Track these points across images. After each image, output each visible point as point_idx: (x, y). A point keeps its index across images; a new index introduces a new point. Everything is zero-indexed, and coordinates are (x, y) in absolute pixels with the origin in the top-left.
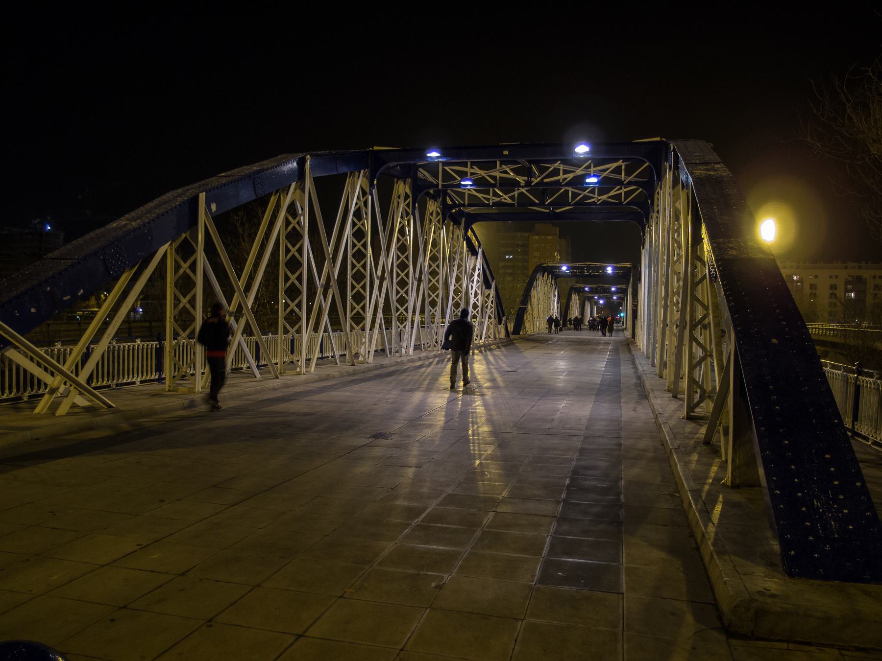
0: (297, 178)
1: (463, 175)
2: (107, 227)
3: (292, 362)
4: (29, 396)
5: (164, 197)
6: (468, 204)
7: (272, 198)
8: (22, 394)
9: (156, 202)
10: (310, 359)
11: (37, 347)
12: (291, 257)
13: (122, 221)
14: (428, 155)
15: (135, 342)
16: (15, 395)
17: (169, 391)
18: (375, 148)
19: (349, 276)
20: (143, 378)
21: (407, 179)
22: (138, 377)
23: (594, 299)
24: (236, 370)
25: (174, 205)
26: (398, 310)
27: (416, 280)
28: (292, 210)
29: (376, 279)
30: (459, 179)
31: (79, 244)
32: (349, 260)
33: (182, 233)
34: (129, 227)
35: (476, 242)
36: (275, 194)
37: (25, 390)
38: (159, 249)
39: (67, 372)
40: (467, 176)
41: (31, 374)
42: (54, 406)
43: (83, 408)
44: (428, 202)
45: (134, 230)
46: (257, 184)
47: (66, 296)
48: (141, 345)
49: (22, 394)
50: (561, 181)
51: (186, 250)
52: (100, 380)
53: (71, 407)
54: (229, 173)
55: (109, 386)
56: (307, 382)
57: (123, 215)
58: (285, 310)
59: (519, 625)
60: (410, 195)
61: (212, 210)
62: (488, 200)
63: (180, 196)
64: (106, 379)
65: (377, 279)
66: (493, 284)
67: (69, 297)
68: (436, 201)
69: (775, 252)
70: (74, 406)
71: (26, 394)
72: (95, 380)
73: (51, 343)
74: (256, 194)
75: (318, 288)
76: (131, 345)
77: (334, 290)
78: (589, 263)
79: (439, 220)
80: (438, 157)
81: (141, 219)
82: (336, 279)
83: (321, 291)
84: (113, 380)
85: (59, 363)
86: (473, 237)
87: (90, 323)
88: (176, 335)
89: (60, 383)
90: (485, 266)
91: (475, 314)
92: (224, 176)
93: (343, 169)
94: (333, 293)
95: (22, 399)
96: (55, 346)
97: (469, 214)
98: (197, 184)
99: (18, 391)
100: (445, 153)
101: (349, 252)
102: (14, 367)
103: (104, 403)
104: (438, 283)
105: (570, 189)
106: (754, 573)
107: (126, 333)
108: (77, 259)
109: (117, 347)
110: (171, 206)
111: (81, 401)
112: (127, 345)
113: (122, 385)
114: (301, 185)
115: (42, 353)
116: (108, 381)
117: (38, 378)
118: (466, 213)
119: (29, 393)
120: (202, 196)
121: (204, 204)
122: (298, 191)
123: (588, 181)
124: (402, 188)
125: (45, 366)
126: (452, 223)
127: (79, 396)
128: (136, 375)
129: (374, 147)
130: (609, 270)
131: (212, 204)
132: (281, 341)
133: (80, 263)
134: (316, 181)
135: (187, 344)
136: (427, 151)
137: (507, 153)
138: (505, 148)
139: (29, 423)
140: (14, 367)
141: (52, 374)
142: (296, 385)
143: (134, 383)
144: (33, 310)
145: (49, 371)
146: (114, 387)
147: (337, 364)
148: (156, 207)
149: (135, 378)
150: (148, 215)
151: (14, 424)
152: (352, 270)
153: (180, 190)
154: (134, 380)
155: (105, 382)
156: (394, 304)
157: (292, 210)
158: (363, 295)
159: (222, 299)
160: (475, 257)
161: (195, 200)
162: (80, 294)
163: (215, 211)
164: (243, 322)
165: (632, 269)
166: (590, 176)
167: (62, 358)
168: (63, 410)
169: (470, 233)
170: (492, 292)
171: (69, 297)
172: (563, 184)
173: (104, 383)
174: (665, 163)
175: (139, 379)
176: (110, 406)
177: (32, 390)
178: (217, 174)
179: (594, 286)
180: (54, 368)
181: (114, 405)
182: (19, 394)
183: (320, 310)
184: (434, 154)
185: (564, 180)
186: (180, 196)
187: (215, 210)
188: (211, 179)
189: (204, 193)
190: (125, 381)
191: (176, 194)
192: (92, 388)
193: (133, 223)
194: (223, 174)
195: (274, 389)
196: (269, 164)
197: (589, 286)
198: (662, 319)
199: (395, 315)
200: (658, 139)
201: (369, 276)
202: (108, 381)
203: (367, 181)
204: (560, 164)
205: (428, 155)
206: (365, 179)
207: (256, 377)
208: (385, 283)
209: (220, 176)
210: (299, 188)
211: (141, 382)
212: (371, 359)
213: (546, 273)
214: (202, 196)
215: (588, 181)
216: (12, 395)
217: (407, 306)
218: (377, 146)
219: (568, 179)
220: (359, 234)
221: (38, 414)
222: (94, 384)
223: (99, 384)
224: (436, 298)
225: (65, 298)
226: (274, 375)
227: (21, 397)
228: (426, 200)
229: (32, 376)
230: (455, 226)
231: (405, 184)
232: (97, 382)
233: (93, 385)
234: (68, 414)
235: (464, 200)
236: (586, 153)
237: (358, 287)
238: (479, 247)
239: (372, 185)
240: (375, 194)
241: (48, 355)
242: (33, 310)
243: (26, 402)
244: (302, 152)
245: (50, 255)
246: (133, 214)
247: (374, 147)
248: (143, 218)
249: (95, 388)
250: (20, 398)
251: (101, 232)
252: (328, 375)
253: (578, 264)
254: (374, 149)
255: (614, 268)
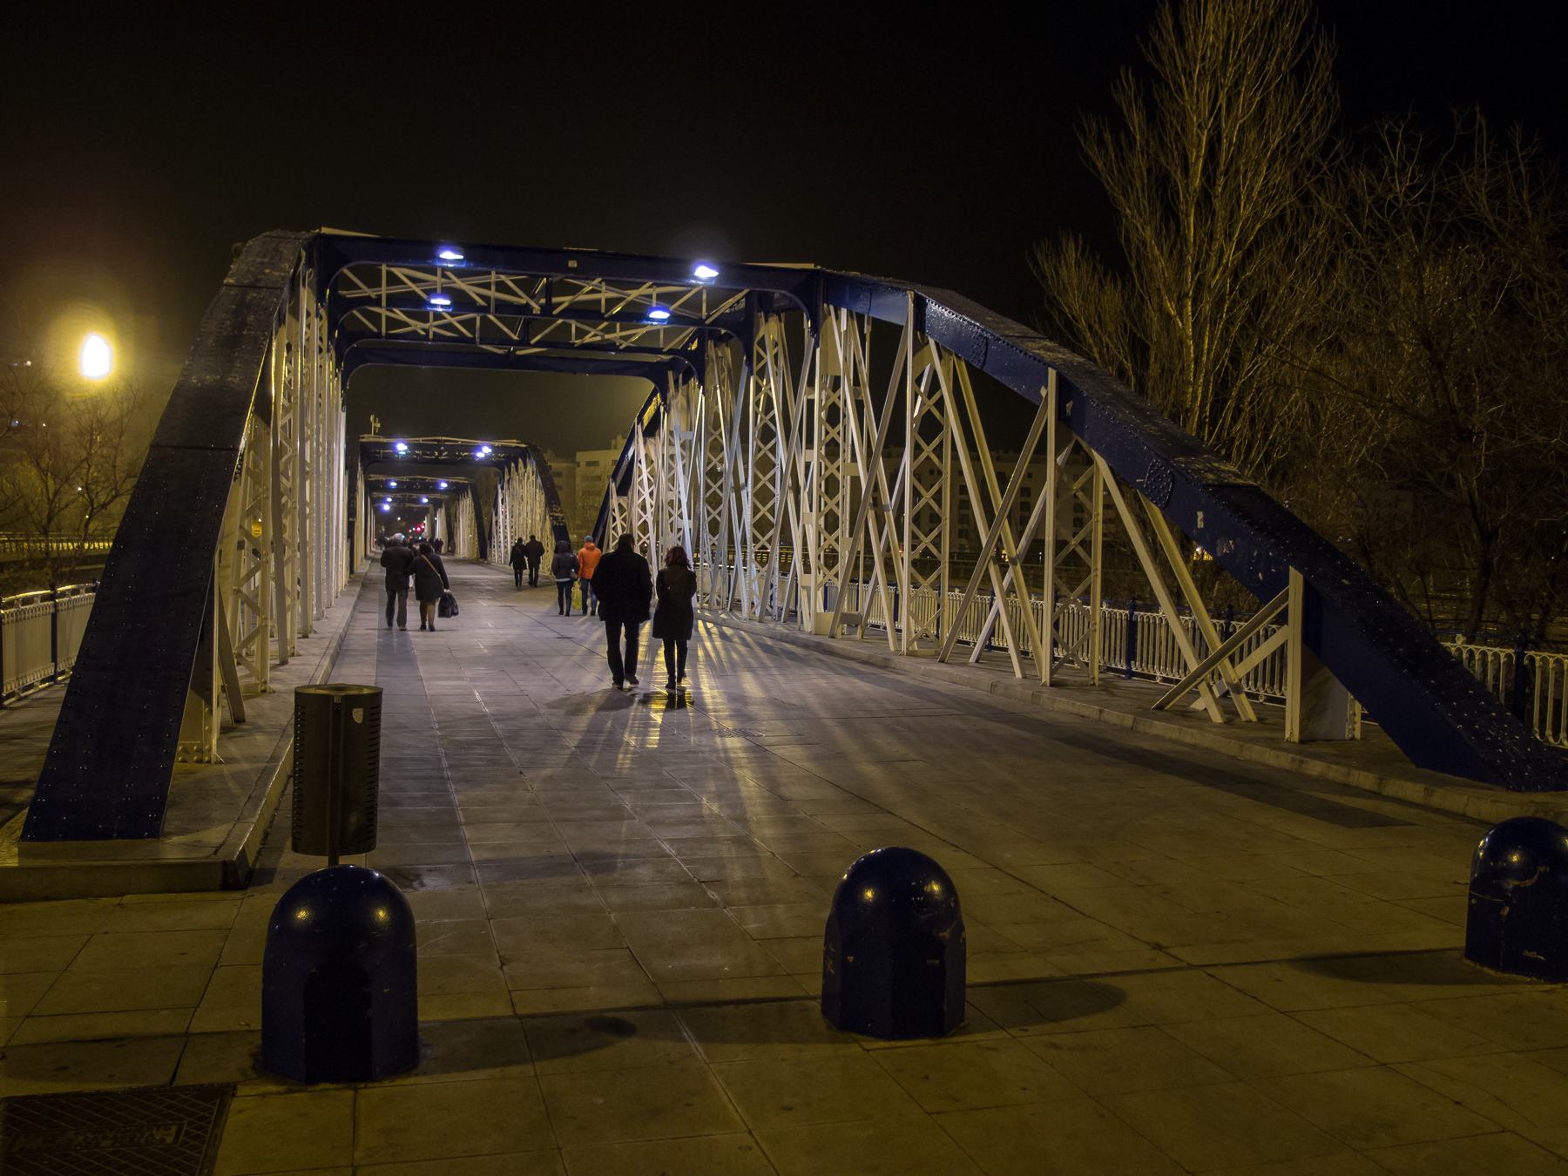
10: (852, 581)
12: (768, 473)
23: (392, 498)
24: (293, 655)
47: (1205, 519)
59: (486, 901)
69: (171, 373)
78: (443, 438)
105: (574, 324)
106: (517, 826)
130: (402, 448)
137: (576, 266)
138: (573, 255)
172: (606, 316)
174: (825, 305)
179: (405, 479)
197: (397, 479)
198: (308, 521)
199: (775, 533)
200: (811, 266)
204: (600, 282)
213: (520, 460)
236: (711, 279)
240: (803, 383)
253: (421, 439)
255: (412, 446)
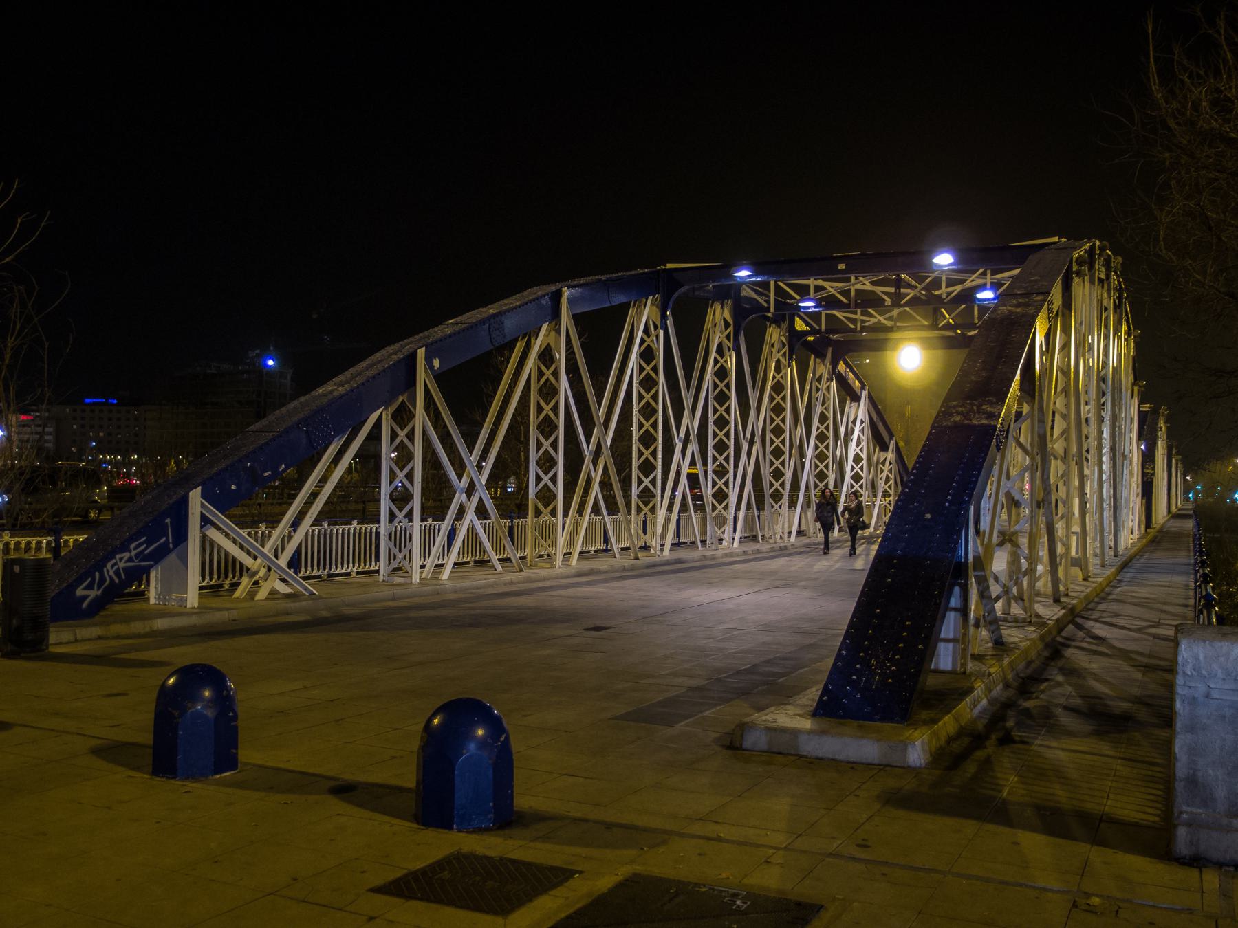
0: (550, 317)
1: (804, 292)
2: (313, 393)
3: (548, 556)
4: (230, 584)
5: (378, 356)
6: (825, 329)
7: (518, 344)
8: (223, 581)
9: (368, 361)
11: (240, 528)
13: (329, 387)
14: (736, 274)
15: (351, 524)
16: (216, 582)
17: (384, 581)
18: (669, 266)
19: (634, 438)
20: (360, 569)
21: (726, 301)
22: (354, 567)
25: (387, 365)
26: (771, 485)
27: (746, 441)
28: (547, 356)
29: (677, 441)
30: (798, 297)
31: (282, 414)
32: (634, 417)
33: (399, 394)
34: (335, 394)
35: (857, 382)
36: (523, 339)
37: (226, 577)
38: (368, 418)
39: (268, 554)
40: (809, 295)
41: (233, 557)
42: (252, 594)
43: (284, 594)
44: (768, 329)
45: (341, 397)
46: (493, 331)
47: (267, 471)
48: (358, 529)
49: (223, 581)
50: (944, 296)
51: (403, 416)
52: (309, 568)
53: (270, 594)
54: (459, 319)
55: (319, 577)
56: (557, 578)
57: (331, 379)
58: (537, 485)
60: (731, 323)
61: (434, 367)
62: (854, 321)
63: (395, 353)
64: (315, 567)
65: (680, 441)
66: (892, 443)
67: (270, 473)
68: (779, 326)
70: (274, 592)
71: (228, 582)
72: (303, 569)
73: (254, 524)
74: (492, 343)
75: (586, 456)
76: (346, 527)
77: (606, 458)
79: (785, 353)
80: (749, 276)
81: (349, 383)
82: (609, 446)
83: (589, 460)
84: (324, 570)
85: (257, 542)
86: (851, 374)
87: (290, 504)
88: (392, 517)
89: (260, 566)
90: (875, 416)
91: (857, 491)
92: (452, 324)
93: (618, 299)
94: (606, 462)
95: (223, 587)
96: (259, 528)
97: (836, 341)
98: (417, 337)
99: (219, 578)
100: (758, 269)
101: (634, 407)
102: (270, 596)
103: (306, 589)
104: (784, 445)
107: (332, 513)
108: (278, 432)
109: (329, 530)
110: (383, 367)
111: (283, 588)
112: (341, 528)
113: (338, 575)
114: (556, 326)
115: (245, 535)
116: (318, 570)
117: (225, 551)
118: (834, 340)
119: (231, 580)
120: (421, 352)
121: (423, 361)
122: (553, 333)
123: (980, 295)
124: (719, 315)
125: (240, 543)
126: (813, 356)
127: (278, 580)
128: (351, 565)
129: (668, 265)
131: (434, 361)
132: (532, 525)
133: (281, 436)
134: (577, 318)
135: (405, 528)
136: (732, 269)
137: (844, 267)
138: (841, 259)
139: (228, 605)
140: (270, 596)
141: (255, 558)
142: (544, 580)
143: (349, 574)
144: (233, 487)
145: (252, 555)
146: (326, 577)
147: (615, 557)
148: (367, 369)
149: (350, 568)
150: (357, 379)
151: (213, 605)
152: (639, 430)
153: (396, 346)
154: (349, 571)
155: (314, 571)
156: (767, 477)
157: (547, 356)
158: (653, 464)
159: (451, 471)
160: (857, 404)
161: (413, 357)
162: (281, 469)
163: (438, 369)
164: (475, 500)
165: (1149, 415)
166: (983, 287)
167: (263, 540)
168: (262, 595)
169: (841, 367)
170: (890, 455)
171: (270, 473)
173: (314, 573)
175: (355, 570)
176: (313, 594)
177: (234, 577)
178: (444, 322)
180: (293, 577)
181: (317, 593)
182: (220, 582)
183: (589, 482)
184: (744, 273)
185: (948, 294)
186: (395, 353)
187: (438, 366)
188: (436, 329)
189: (424, 348)
190: (337, 572)
191: (391, 351)
192: (300, 577)
193: (340, 389)
194: (452, 321)
195: (511, 583)
196: (511, 303)
201: (788, 430)
202: (318, 570)
203: (658, 310)
205: (736, 274)
206: (654, 308)
207: (496, 570)
208: (754, 448)
209: (448, 325)
210: (554, 330)
211: (358, 573)
212: (666, 551)
214: (421, 352)
215: (980, 295)
216: (212, 583)
217: (783, 481)
218: (670, 263)
219: (953, 294)
220: (721, 373)
221: (238, 598)
222: (302, 573)
223: (308, 574)
224: (855, 466)
225: (266, 474)
226: (516, 566)
227: (223, 584)
228: (766, 325)
229: (234, 560)
230: (818, 360)
231: (722, 307)
232: (306, 571)
233: (301, 575)
234: (266, 599)
235: (820, 325)
237: (647, 453)
238: (863, 388)
239: (664, 316)
241: (251, 537)
242: (233, 487)
243: (227, 590)
244: (553, 282)
245: (251, 428)
246: (341, 378)
247: (668, 265)
248: (352, 382)
249: (304, 578)
250: (221, 586)
251: (294, 408)
252: (592, 569)
254: (667, 267)
